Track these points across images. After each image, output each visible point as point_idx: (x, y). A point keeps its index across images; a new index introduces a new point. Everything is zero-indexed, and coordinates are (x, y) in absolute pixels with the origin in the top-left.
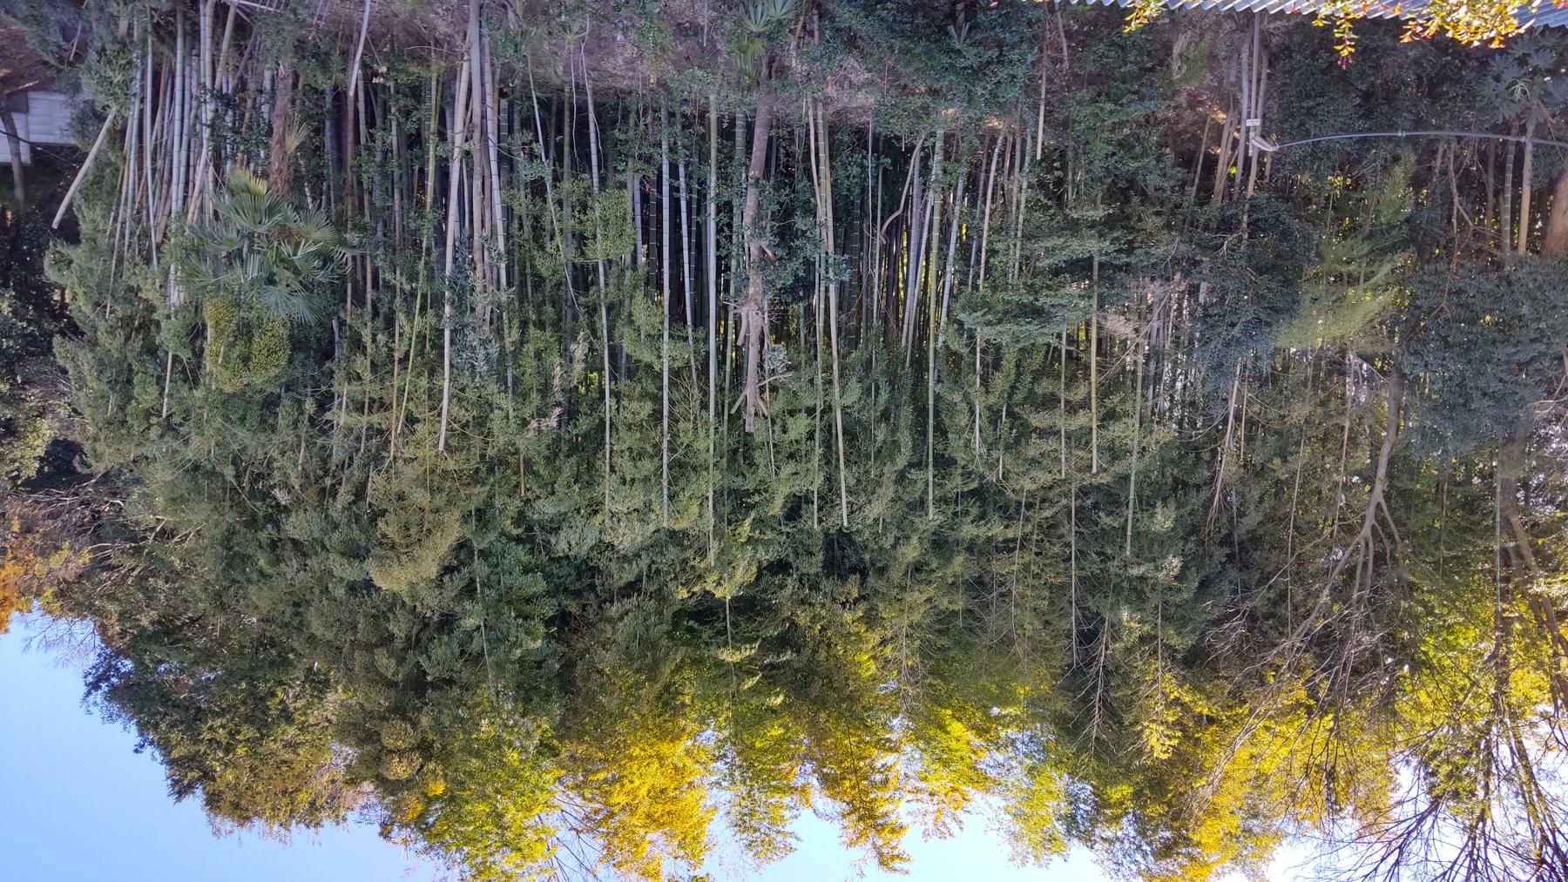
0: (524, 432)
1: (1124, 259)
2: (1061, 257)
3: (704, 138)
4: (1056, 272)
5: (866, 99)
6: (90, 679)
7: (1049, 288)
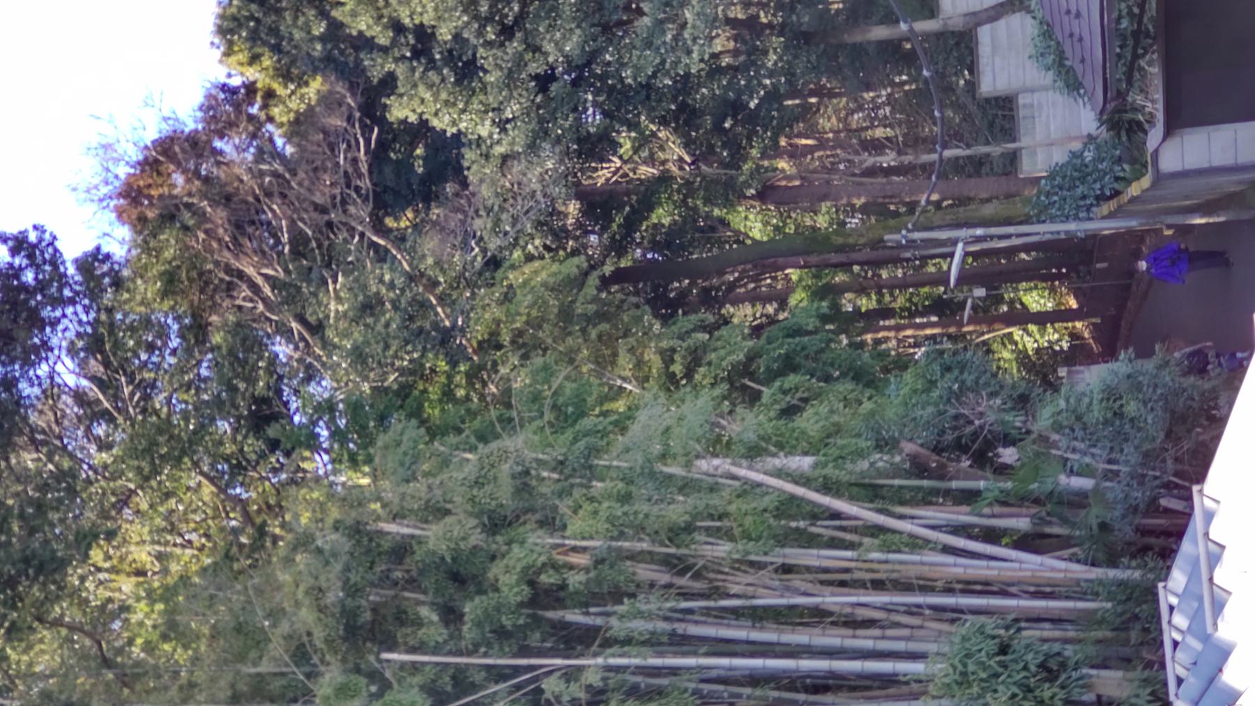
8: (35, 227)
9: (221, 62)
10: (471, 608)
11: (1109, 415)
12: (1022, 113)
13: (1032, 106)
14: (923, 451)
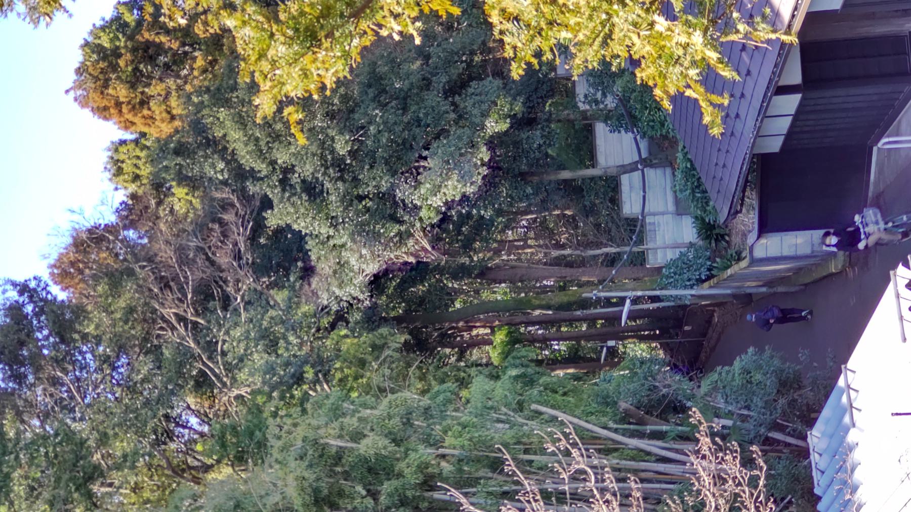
6: (33, 284)
8: (35, 278)
9: (110, 180)
10: (387, 487)
11: (745, 382)
12: (648, 228)
13: (654, 223)
14: (631, 407)
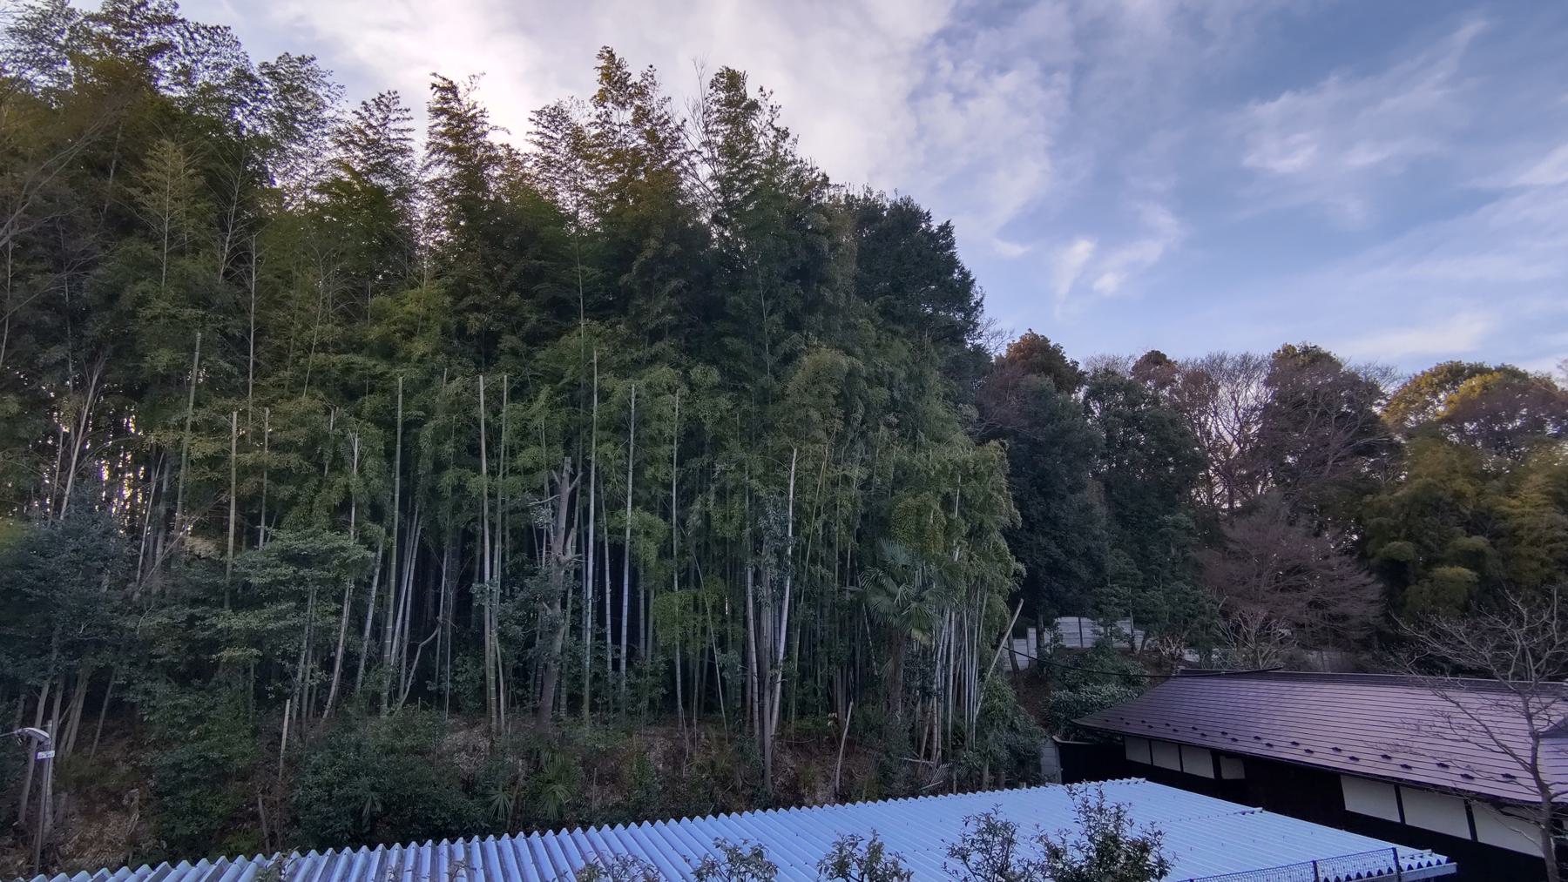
0: (737, 462)
1: (197, 611)
2: (270, 610)
3: (594, 695)
4: (274, 599)
5: (459, 737)
7: (282, 583)
